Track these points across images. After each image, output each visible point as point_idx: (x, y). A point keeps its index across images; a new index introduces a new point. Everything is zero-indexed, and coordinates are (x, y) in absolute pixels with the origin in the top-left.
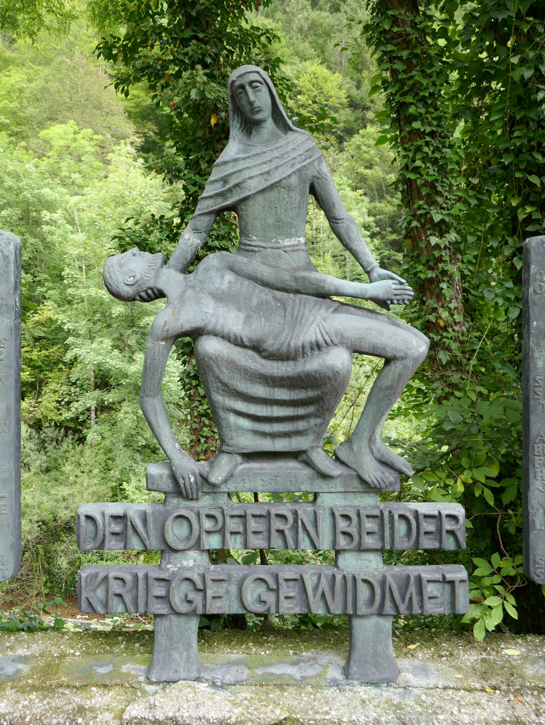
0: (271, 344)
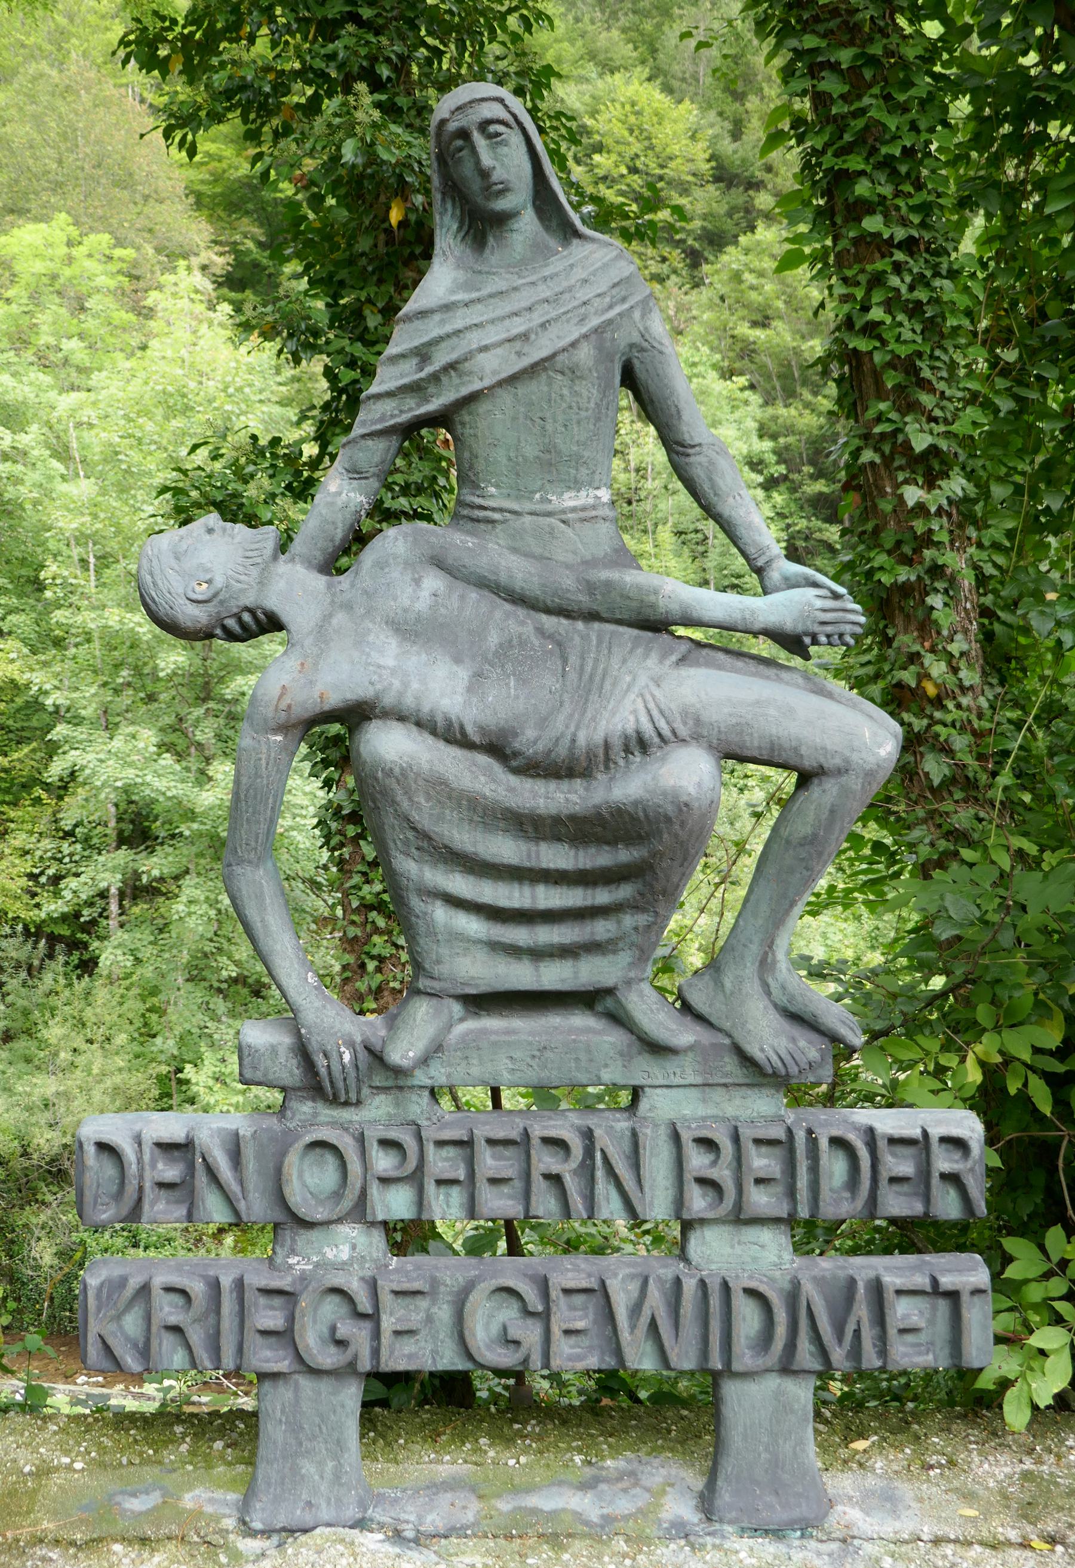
0: (531, 740)
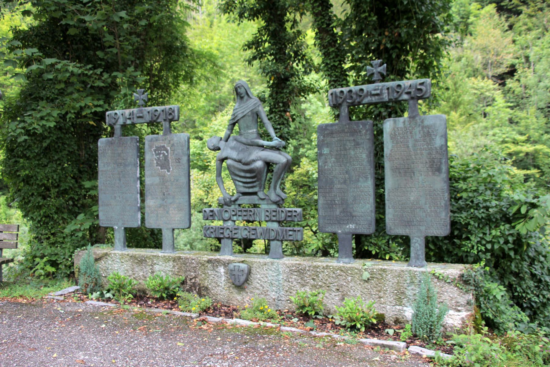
0: (243, 161)
